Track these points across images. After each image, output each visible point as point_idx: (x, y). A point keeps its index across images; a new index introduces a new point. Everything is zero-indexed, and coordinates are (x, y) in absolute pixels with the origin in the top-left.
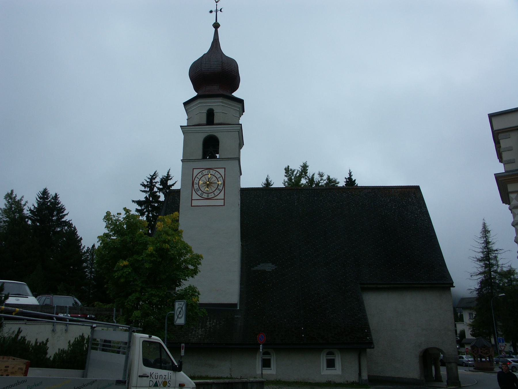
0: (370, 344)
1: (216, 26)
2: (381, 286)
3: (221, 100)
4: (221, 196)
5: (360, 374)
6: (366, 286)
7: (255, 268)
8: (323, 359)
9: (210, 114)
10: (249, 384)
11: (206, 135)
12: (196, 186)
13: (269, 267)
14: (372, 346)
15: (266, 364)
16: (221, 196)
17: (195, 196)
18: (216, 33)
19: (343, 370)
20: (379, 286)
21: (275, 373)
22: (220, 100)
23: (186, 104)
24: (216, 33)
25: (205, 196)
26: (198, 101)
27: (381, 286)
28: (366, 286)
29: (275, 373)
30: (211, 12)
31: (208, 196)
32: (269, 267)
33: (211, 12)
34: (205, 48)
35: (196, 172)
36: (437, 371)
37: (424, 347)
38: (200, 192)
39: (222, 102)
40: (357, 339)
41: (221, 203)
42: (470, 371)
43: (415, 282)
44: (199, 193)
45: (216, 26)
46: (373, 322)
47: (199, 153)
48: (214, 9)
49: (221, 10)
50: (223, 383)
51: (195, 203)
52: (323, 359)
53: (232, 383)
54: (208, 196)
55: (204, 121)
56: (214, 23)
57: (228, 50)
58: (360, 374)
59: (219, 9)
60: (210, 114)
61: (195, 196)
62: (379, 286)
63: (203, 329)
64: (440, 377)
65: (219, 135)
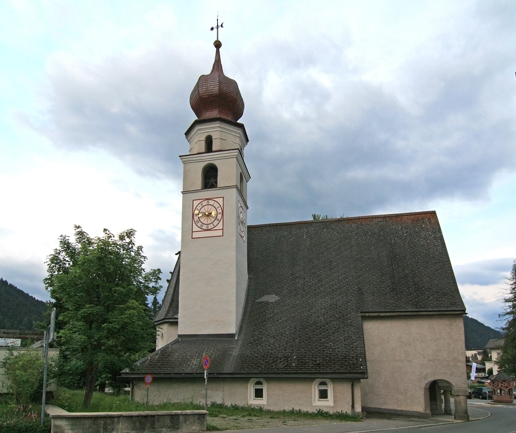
0: (364, 374)
1: (218, 45)
2: (384, 314)
3: (218, 125)
4: (220, 226)
5: (353, 406)
6: (367, 314)
7: (443, 409)
8: (315, 389)
9: (209, 141)
10: (181, 417)
11: (206, 163)
12: (196, 218)
13: (272, 298)
14: (366, 377)
15: (259, 394)
16: (220, 226)
17: (195, 228)
18: (218, 53)
19: (335, 401)
20: (381, 314)
21: (266, 403)
22: (217, 124)
23: (187, 133)
24: (218, 53)
25: (205, 227)
26: (197, 128)
27: (384, 314)
28: (367, 314)
29: (266, 403)
30: (212, 29)
31: (207, 227)
32: (272, 298)
33: (212, 29)
34: (207, 70)
35: (196, 203)
36: (447, 401)
37: (431, 379)
38: (200, 223)
39: (220, 127)
40: (351, 369)
41: (220, 233)
42: (489, 403)
43: (420, 310)
44: (199, 224)
45: (218, 45)
46: (373, 352)
47: (198, 182)
48: (215, 26)
49: (222, 26)
50: (138, 416)
51: (195, 235)
52: (315, 389)
53: (153, 416)
54: (207, 227)
55: (203, 150)
56: (216, 41)
57: (229, 71)
58: (353, 406)
59: (220, 24)
60: (209, 141)
61: (195, 228)
62: (381, 314)
63: (199, 360)
64: (450, 410)
65: (216, 163)
